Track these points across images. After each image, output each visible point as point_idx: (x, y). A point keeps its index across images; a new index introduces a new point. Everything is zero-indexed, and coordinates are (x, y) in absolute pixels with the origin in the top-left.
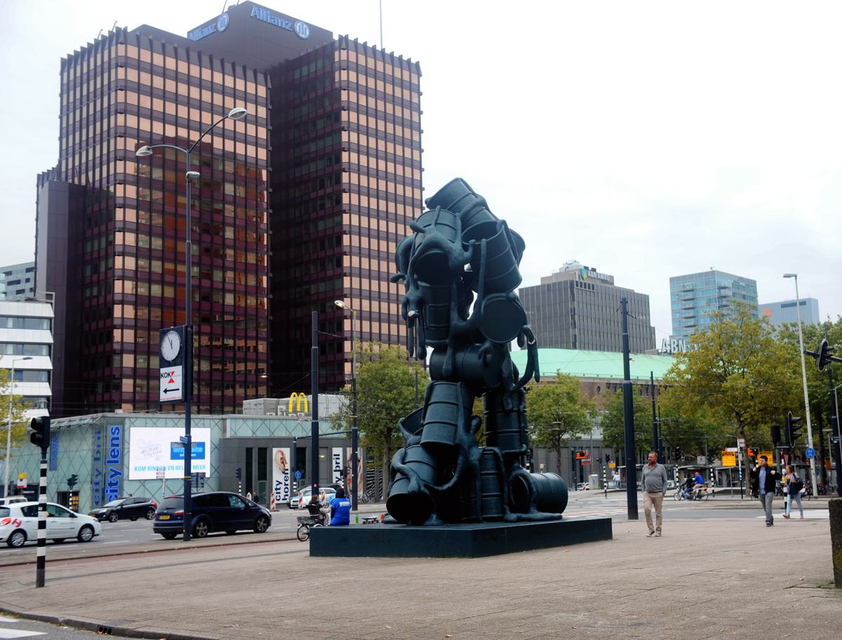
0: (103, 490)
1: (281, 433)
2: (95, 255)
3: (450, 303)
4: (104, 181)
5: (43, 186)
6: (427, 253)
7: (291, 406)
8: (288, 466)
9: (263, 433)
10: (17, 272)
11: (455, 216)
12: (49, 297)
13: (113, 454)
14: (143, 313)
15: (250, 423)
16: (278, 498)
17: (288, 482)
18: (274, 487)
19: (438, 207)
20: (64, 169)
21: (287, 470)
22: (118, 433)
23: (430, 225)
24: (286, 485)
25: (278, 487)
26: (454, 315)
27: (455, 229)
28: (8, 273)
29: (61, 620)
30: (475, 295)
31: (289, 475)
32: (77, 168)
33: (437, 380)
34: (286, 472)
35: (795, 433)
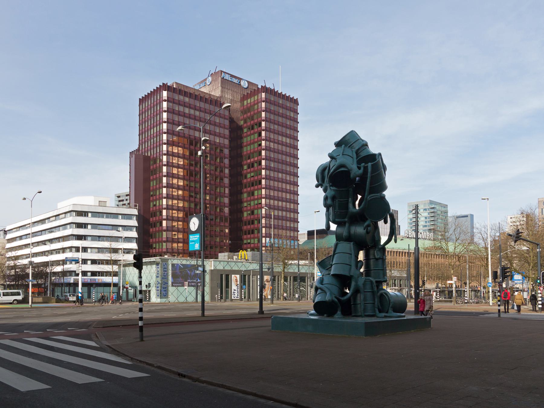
0: (161, 290)
1: (235, 268)
2: (154, 188)
3: (348, 198)
4: (158, 154)
5: (132, 157)
6: (338, 171)
7: (240, 255)
8: (238, 283)
9: (228, 268)
10: (122, 196)
11: (352, 151)
12: (136, 206)
13: (164, 275)
14: (186, 205)
15: (222, 263)
16: (234, 297)
17: (239, 290)
18: (233, 292)
19: (343, 146)
20: (141, 149)
21: (238, 284)
22: (166, 266)
23: (340, 155)
24: (237, 291)
25: (234, 292)
26: (350, 205)
27: (352, 158)
28: (119, 197)
29: (155, 365)
30: (359, 197)
31: (239, 287)
32: (146, 148)
33: (340, 241)
34: (238, 285)
35: (505, 275)
